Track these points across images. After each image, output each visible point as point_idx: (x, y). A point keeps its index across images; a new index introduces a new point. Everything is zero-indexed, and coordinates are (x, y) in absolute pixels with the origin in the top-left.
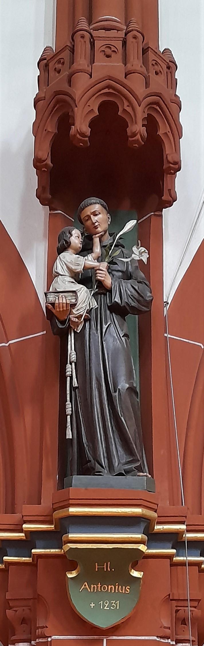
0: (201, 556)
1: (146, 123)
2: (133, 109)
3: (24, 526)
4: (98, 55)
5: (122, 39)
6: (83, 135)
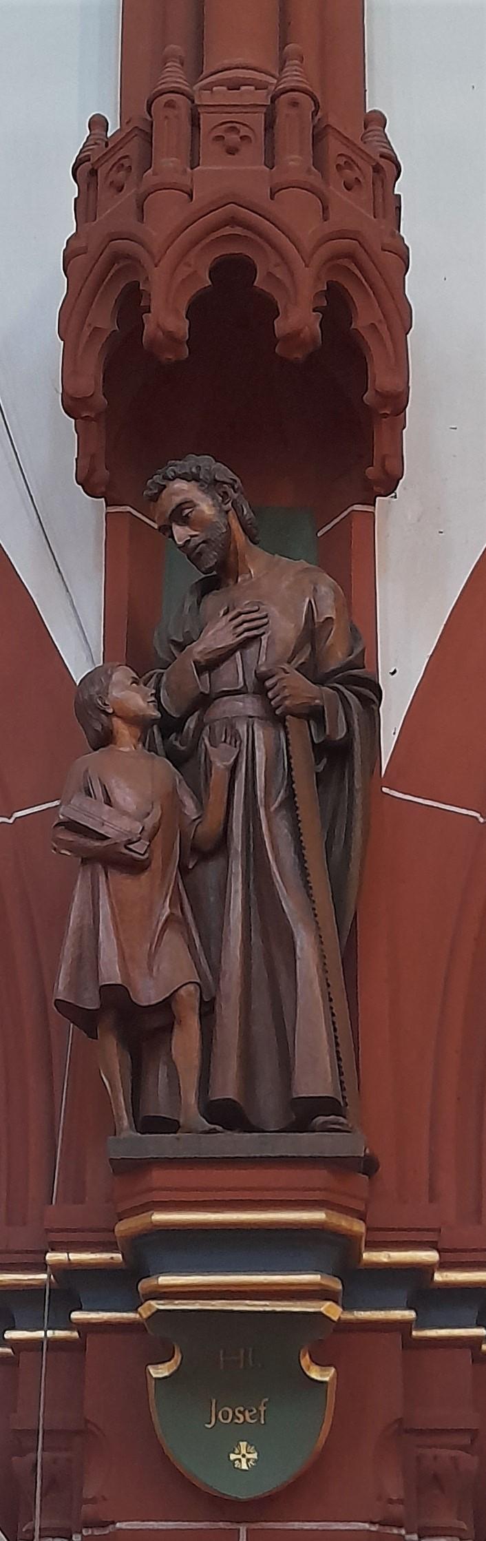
0: (478, 1325)
1: (325, 304)
2: (291, 273)
3: (51, 1257)
4: (207, 146)
5: (264, 110)
6: (170, 335)
